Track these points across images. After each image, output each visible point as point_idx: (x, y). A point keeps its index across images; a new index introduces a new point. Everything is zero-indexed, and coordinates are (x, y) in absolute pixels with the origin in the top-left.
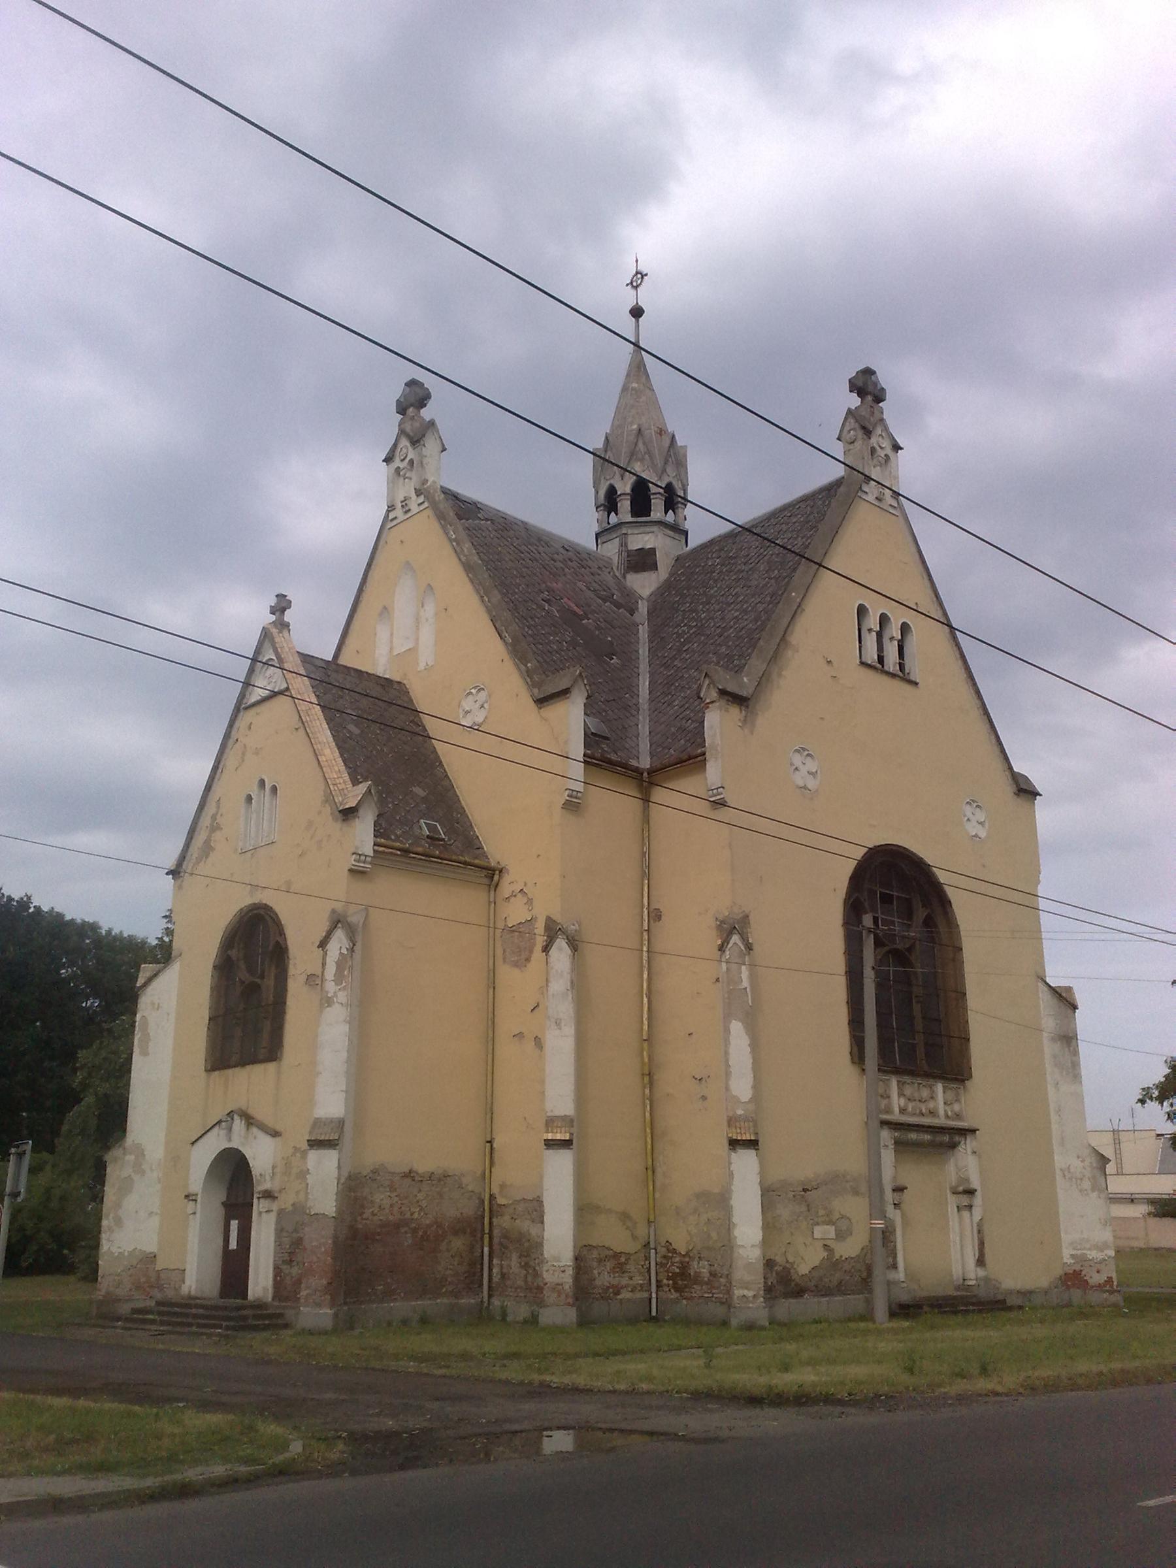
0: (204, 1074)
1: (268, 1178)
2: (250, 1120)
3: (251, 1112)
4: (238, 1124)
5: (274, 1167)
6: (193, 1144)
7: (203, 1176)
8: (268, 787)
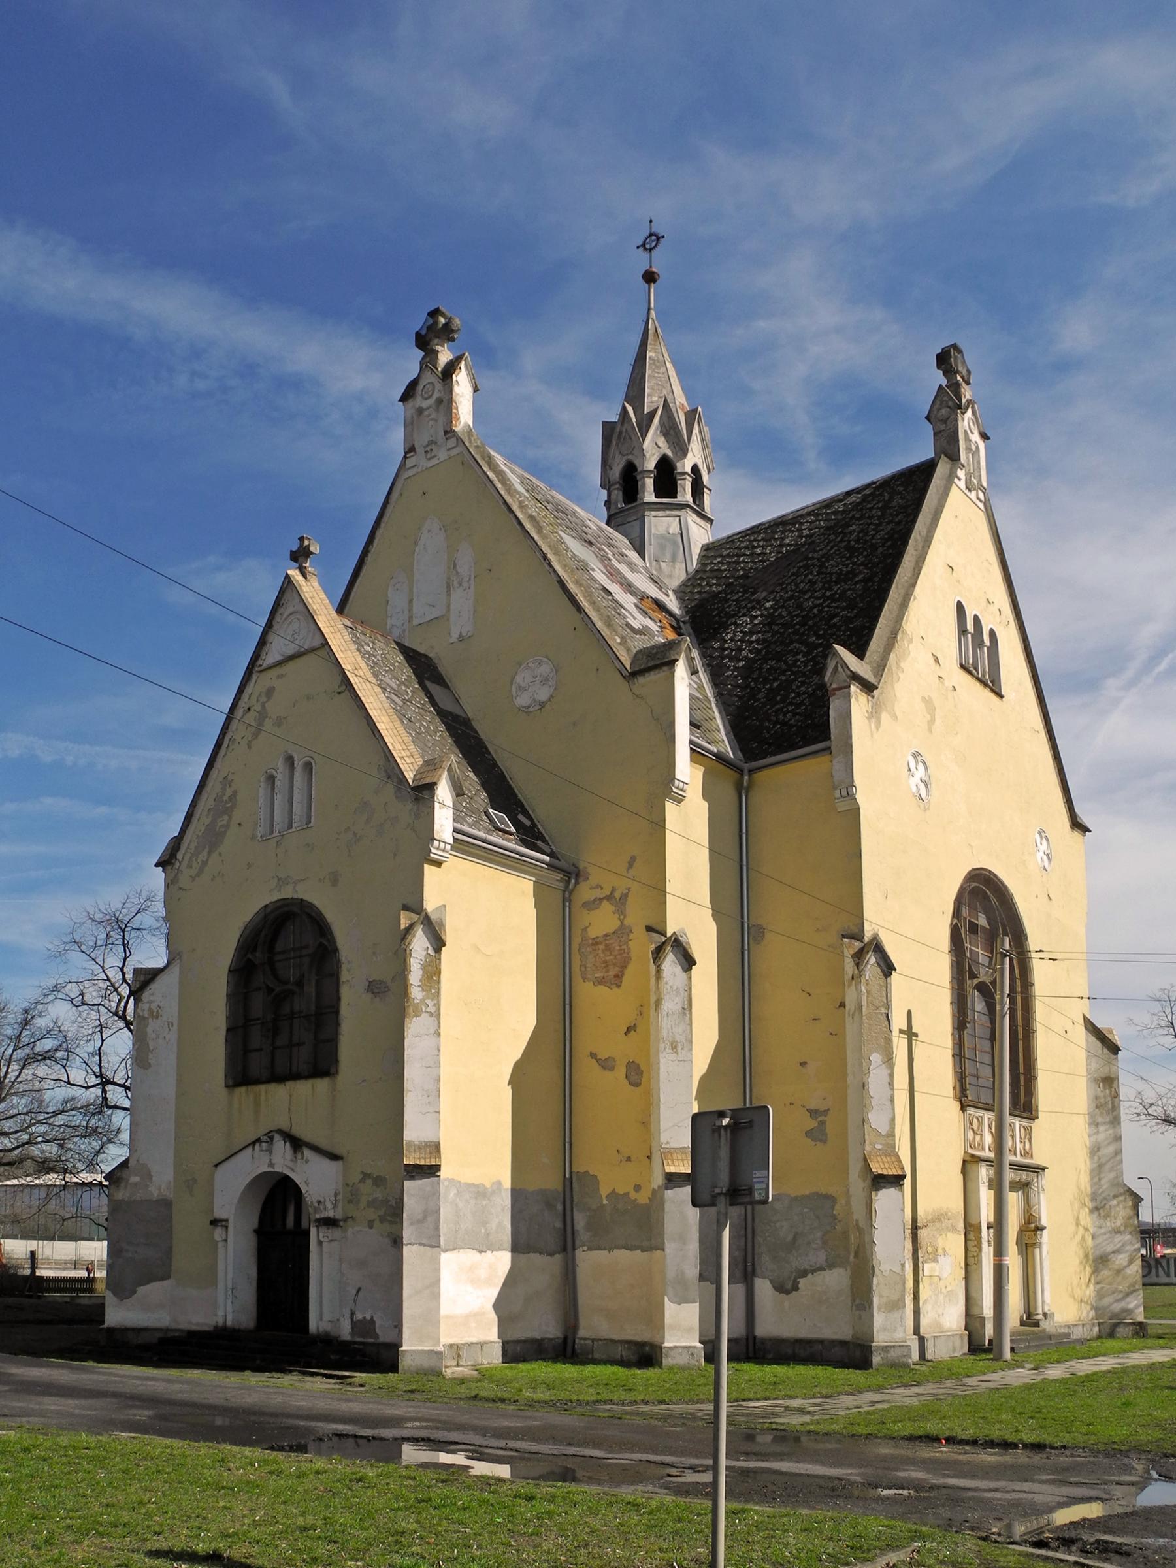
0: (223, 1092)
1: (329, 1205)
2: (297, 1144)
3: (297, 1131)
4: (281, 1148)
5: (336, 1195)
6: (216, 1166)
7: (235, 1201)
8: (298, 764)
